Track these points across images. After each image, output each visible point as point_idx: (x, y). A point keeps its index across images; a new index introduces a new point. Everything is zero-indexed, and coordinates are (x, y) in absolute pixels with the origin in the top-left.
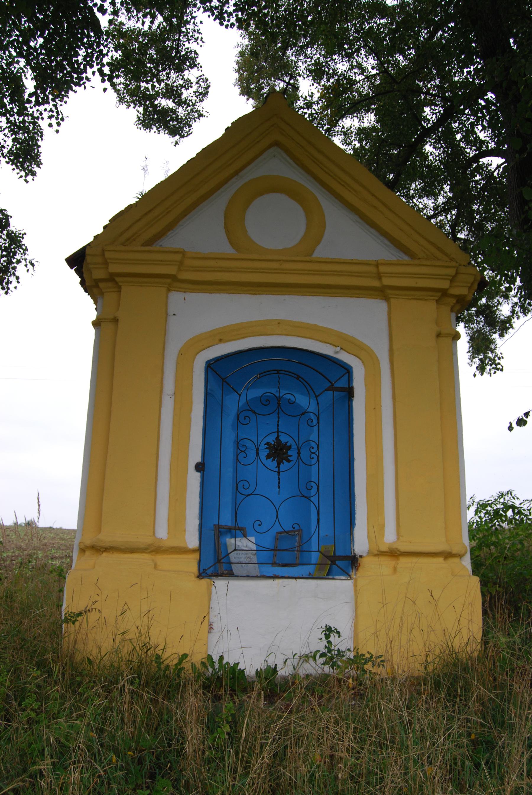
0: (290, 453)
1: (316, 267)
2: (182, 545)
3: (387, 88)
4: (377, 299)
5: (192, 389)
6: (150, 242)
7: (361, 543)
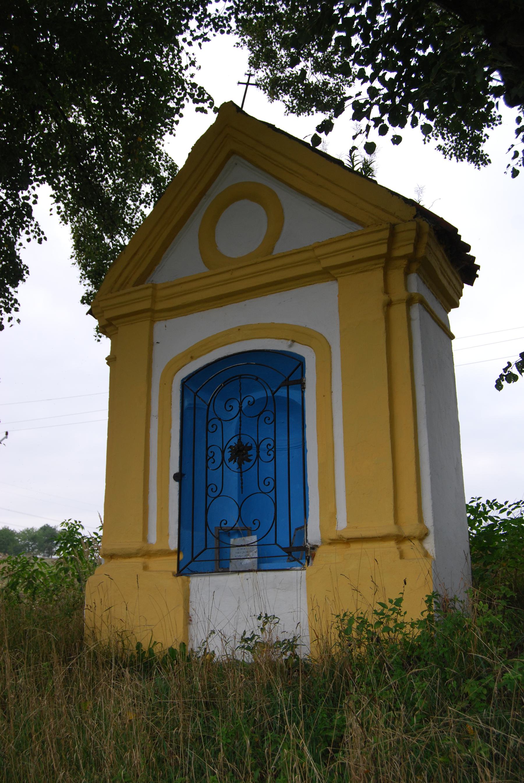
0: (250, 453)
1: (280, 262)
2: (165, 548)
3: (480, 33)
4: (328, 281)
5: (171, 408)
6: (141, 281)
7: (313, 534)
